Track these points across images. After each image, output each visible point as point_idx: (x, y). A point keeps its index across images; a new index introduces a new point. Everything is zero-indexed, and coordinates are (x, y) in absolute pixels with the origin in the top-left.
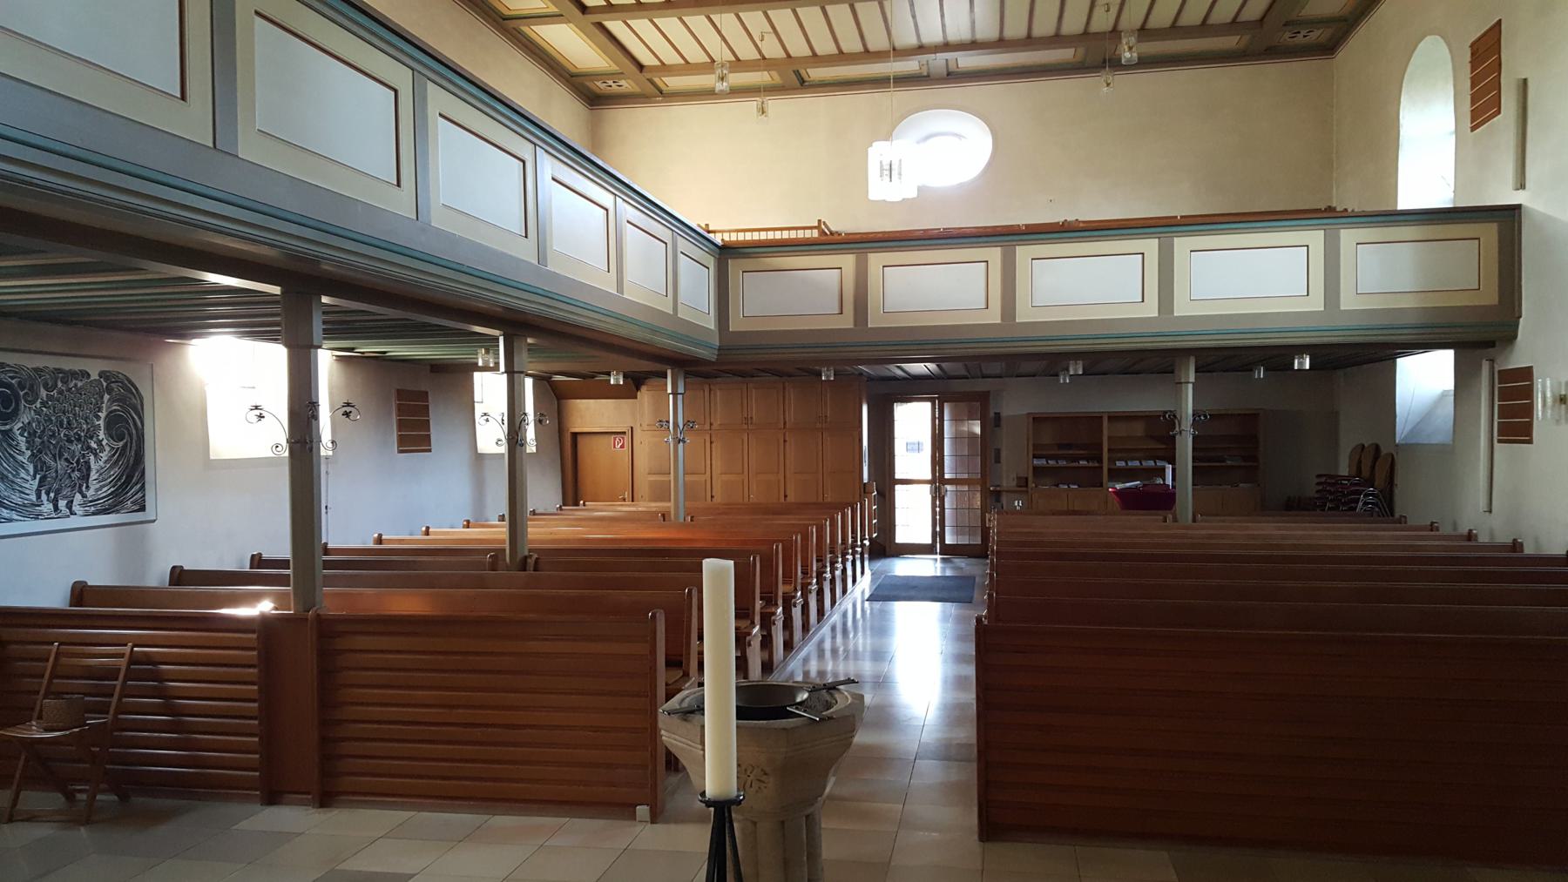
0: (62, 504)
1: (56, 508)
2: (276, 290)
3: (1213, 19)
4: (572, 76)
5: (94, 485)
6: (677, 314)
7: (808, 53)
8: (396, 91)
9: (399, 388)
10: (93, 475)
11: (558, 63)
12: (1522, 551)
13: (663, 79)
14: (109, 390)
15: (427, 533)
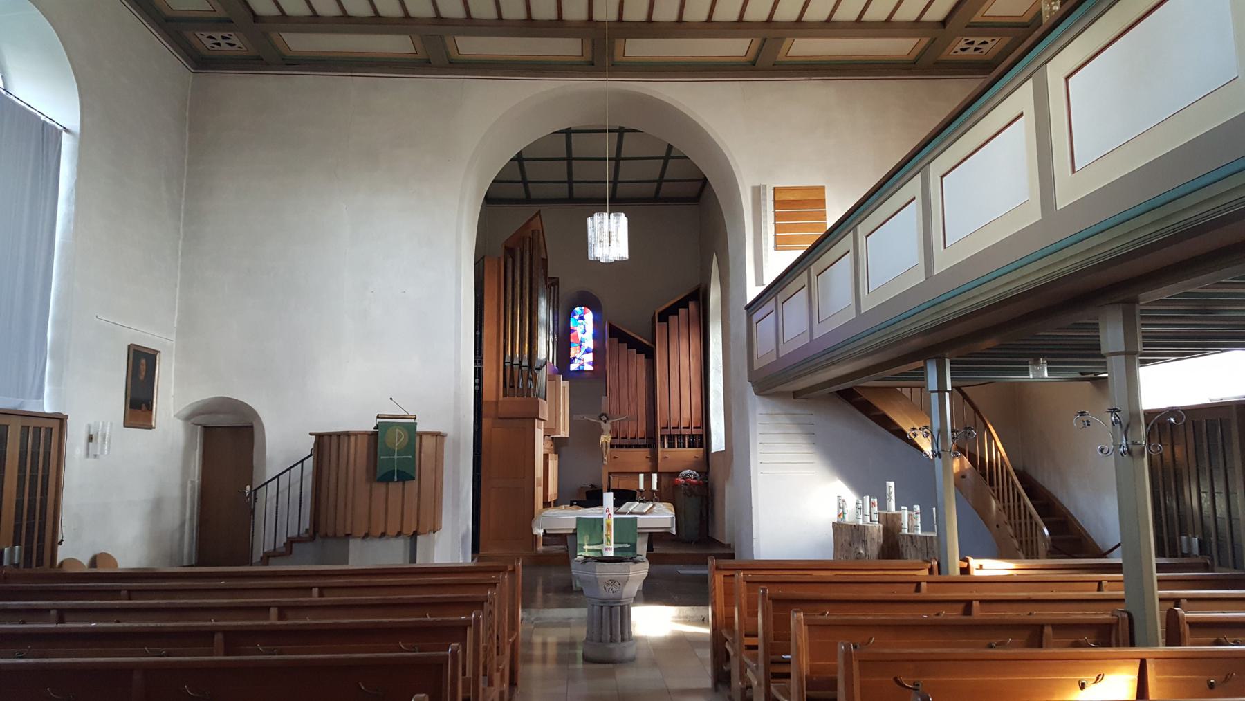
3: (898, 17)
4: (167, 21)
7: (494, 15)
8: (1067, 78)
12: (947, 573)
13: (282, 35)
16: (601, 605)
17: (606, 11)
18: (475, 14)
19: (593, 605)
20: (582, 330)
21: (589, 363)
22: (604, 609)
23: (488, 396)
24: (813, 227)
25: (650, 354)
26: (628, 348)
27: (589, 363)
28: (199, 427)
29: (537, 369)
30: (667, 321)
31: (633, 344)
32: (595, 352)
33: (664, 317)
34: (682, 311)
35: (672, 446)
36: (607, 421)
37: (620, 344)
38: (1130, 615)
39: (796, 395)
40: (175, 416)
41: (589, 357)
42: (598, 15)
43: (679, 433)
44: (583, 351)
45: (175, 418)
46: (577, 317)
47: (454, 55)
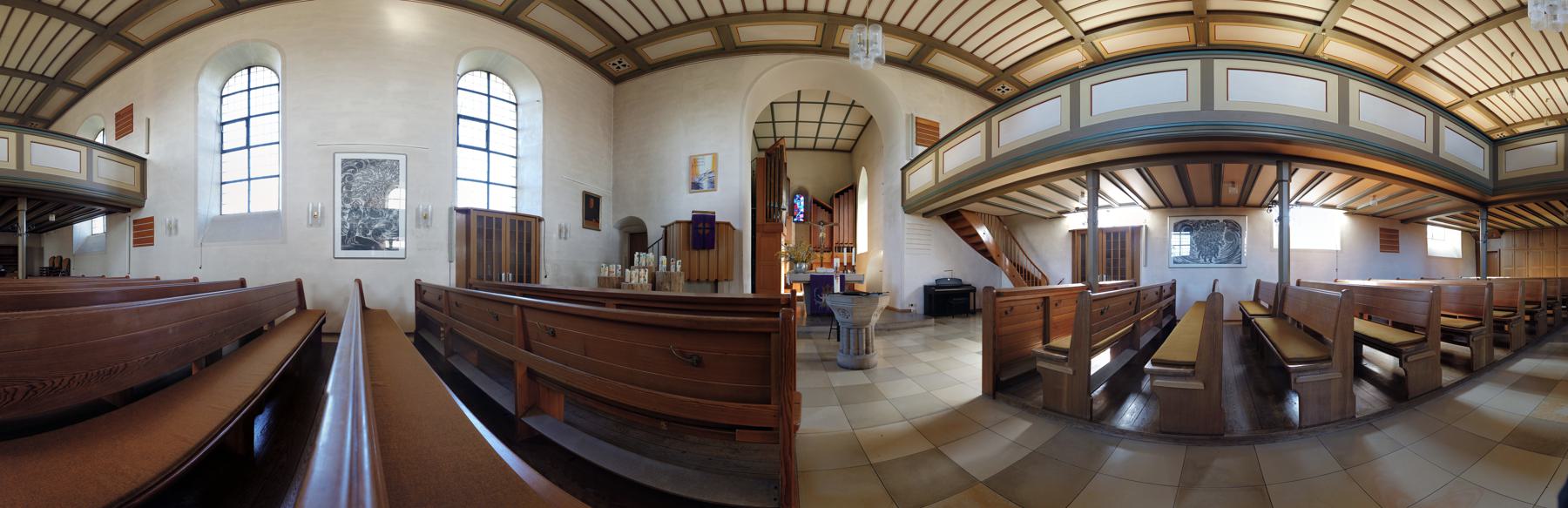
0: (1207, 260)
1: (1205, 261)
2: (864, 172)
5: (1220, 254)
6: (1438, 154)
9: (1382, 227)
10: (1220, 252)
11: (896, 59)
14: (1227, 226)
15: (1336, 281)
17: (837, 6)
18: (749, 8)
19: (849, 329)
22: (851, 331)
23: (758, 222)
24: (934, 138)
25: (831, 212)
31: (823, 207)
32: (804, 213)
33: (837, 196)
38: (359, 282)
39: (925, 215)
41: (802, 216)
42: (831, 9)
47: (738, 44)
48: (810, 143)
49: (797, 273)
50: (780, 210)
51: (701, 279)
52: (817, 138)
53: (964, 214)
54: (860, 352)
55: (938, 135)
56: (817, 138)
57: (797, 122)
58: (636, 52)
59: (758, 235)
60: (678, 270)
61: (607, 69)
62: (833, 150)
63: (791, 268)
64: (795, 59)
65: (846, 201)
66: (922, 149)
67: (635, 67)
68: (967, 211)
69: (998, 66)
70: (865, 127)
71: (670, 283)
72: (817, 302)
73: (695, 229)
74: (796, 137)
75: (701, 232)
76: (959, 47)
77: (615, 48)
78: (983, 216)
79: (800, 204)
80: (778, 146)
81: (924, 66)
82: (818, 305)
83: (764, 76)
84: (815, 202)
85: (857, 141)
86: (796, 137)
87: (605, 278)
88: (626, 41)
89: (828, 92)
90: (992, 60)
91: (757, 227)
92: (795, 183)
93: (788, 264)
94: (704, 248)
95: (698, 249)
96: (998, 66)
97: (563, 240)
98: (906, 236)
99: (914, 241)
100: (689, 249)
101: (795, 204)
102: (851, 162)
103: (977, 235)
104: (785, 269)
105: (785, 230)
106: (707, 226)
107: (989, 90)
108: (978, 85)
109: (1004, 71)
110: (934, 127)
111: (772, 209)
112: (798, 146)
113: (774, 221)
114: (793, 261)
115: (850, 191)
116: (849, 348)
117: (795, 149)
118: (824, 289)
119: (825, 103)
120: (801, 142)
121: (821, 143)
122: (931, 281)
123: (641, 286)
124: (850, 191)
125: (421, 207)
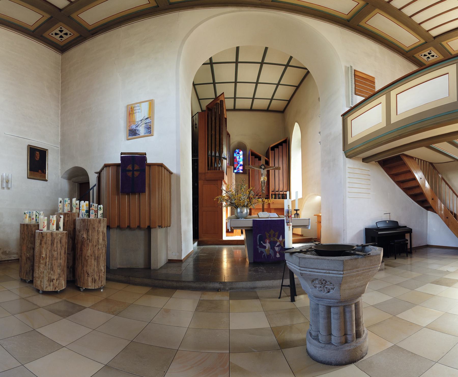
2: (296, 127)
16: (317, 303)
20: (239, 158)
21: (241, 170)
22: (332, 310)
24: (371, 91)
26: (259, 160)
27: (241, 170)
28: (77, 184)
29: (223, 158)
30: (274, 150)
32: (243, 165)
33: (273, 149)
34: (280, 147)
35: (275, 198)
36: (265, 169)
37: (255, 159)
39: (365, 160)
40: (61, 177)
41: (241, 168)
43: (279, 193)
44: (239, 165)
45: (62, 179)
46: (236, 153)
48: (247, 104)
49: (238, 218)
50: (220, 158)
51: (132, 226)
52: (253, 98)
53: (406, 160)
54: (349, 337)
55: (374, 88)
56: (253, 98)
57: (236, 82)
58: (72, 19)
59: (200, 183)
60: (99, 216)
61: (51, 39)
62: (268, 110)
63: (232, 213)
64: (233, 12)
65: (281, 154)
66: (360, 99)
67: (77, 35)
68: (412, 158)
69: (431, 32)
70: (297, 87)
71: (88, 231)
72: (260, 250)
73: (124, 171)
74: (235, 98)
75: (130, 174)
76: (400, 9)
77: (52, 17)
78: (417, 160)
79: (240, 157)
80: (219, 102)
81: (360, 26)
82: (262, 252)
83: (200, 27)
84: (253, 154)
85: (289, 101)
86: (235, 98)
87: (27, 225)
88: (60, 10)
89: (266, 49)
90: (426, 26)
91: (200, 176)
92: (235, 139)
93: (229, 208)
94: (134, 193)
95: (128, 194)
96: (431, 32)
97: (5, 190)
98: (348, 180)
99: (356, 186)
100: (118, 194)
101: (235, 158)
102: (284, 120)
103: (415, 179)
104: (226, 213)
105: (226, 178)
106: (137, 167)
107: (416, 56)
108: (407, 49)
109: (435, 38)
110: (371, 81)
111: (213, 158)
112: (236, 108)
113: (215, 169)
114: (234, 206)
115: (284, 144)
116: (330, 334)
117: (234, 110)
118: (267, 235)
119: (262, 63)
120: (240, 104)
121: (258, 104)
122: (371, 224)
123: (52, 234)
124: (284, 144)
125: (4, 174)
